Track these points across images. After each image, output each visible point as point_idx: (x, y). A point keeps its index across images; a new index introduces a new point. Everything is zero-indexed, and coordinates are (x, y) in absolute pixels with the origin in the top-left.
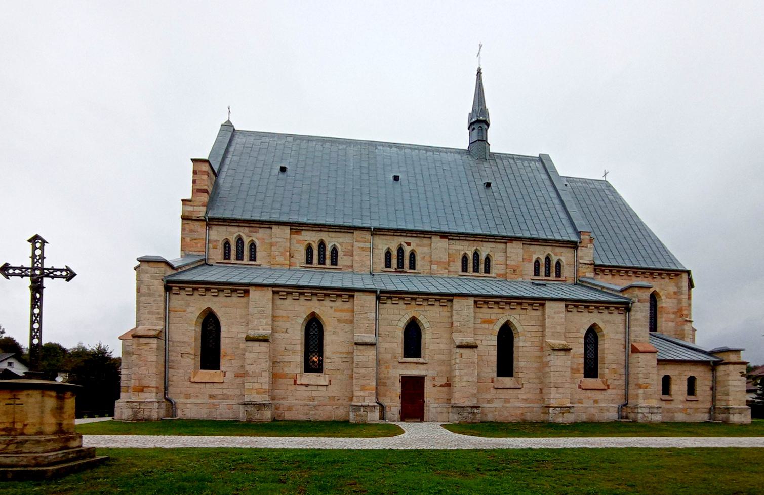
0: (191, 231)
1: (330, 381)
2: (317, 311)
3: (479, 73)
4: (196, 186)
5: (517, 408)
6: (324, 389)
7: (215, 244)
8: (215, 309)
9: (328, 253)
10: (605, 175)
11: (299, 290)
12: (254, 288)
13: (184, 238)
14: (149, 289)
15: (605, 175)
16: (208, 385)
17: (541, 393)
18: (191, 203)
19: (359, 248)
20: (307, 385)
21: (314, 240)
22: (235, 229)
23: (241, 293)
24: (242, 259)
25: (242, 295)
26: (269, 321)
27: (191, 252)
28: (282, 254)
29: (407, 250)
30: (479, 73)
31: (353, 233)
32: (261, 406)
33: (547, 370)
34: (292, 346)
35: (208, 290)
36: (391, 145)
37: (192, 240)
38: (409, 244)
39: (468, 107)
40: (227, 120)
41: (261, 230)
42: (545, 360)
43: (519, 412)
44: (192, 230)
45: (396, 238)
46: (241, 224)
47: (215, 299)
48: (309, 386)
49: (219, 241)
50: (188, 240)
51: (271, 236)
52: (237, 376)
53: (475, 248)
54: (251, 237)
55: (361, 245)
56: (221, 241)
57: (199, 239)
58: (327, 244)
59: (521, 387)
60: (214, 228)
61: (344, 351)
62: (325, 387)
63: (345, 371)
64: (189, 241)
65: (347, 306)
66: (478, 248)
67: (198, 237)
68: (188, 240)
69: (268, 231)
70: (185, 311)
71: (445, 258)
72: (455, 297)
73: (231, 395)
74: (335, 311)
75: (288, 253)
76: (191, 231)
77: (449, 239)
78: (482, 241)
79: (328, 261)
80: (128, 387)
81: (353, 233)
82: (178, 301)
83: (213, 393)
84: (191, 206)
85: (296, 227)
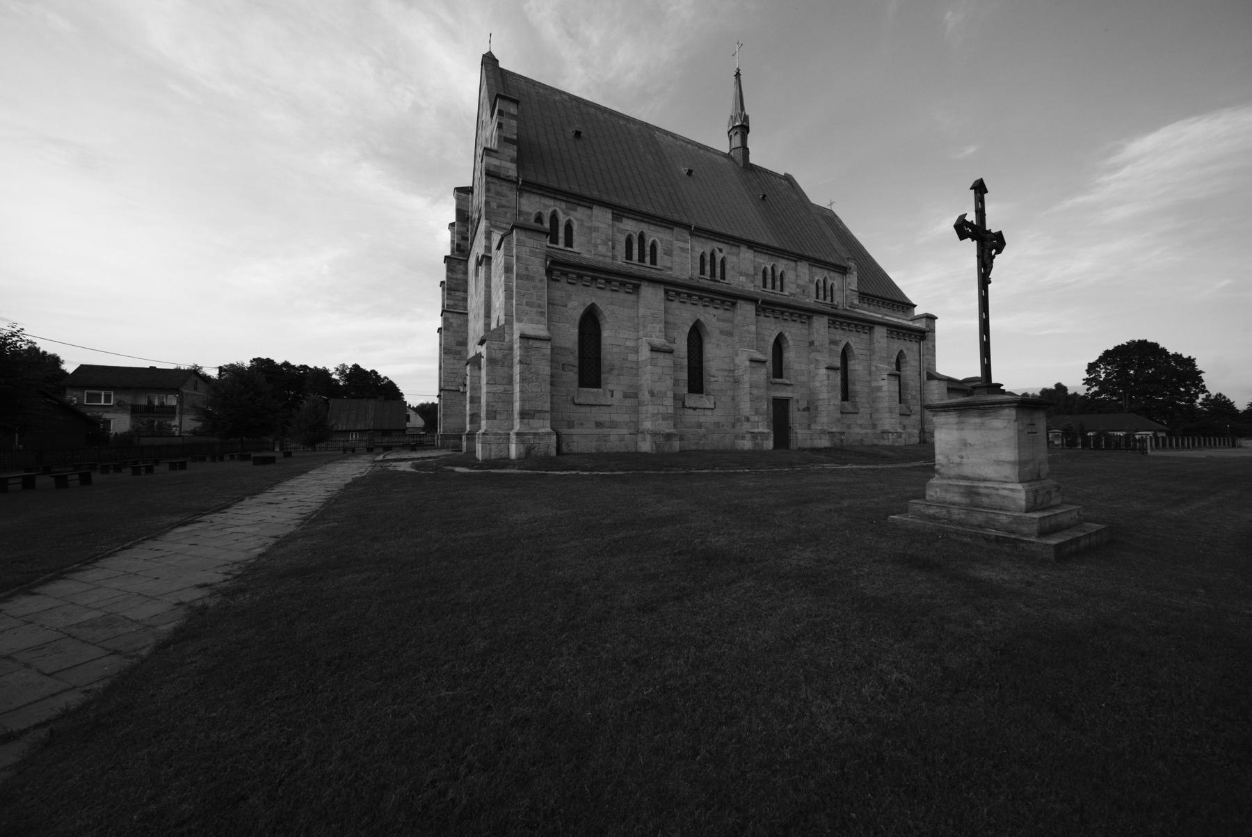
0: (498, 194)
1: (715, 403)
2: (702, 319)
3: (738, 75)
4: (503, 132)
5: (858, 434)
6: (708, 412)
7: (526, 217)
8: (601, 305)
9: (648, 249)
10: (831, 204)
11: (677, 289)
12: (646, 284)
13: (489, 202)
14: (527, 269)
15: (831, 204)
16: (594, 409)
17: (871, 418)
18: (498, 155)
19: (679, 247)
20: (695, 409)
21: (635, 231)
22: (550, 202)
23: (629, 288)
24: (557, 243)
25: (631, 291)
26: (662, 326)
27: (499, 223)
28: (605, 243)
29: (719, 256)
30: (738, 75)
31: (672, 229)
32: (669, 437)
33: (879, 394)
34: (681, 360)
35: (594, 279)
36: (667, 133)
37: (499, 206)
38: (721, 251)
39: (729, 108)
40: (488, 51)
41: (580, 209)
42: (874, 384)
43: (859, 438)
44: (498, 192)
45: (710, 241)
46: (558, 197)
47: (599, 292)
48: (698, 410)
49: (531, 214)
50: (494, 205)
51: (590, 217)
52: (626, 396)
53: (772, 263)
54: (568, 215)
55: (681, 244)
56: (533, 215)
57: (509, 207)
58: (647, 239)
59: (712, 406)
60: (526, 195)
61: (726, 367)
62: (711, 411)
63: (729, 391)
64: (495, 207)
65: (728, 315)
66: (776, 263)
67: (507, 204)
68: (494, 205)
69: (587, 212)
70: (566, 306)
71: (751, 271)
72: (814, 315)
73: (620, 422)
74: (718, 320)
75: (610, 243)
76: (498, 194)
77: (755, 251)
78: (778, 256)
79: (648, 259)
80: (496, 411)
81: (672, 229)
82: (563, 289)
83: (601, 419)
84: (498, 159)
85: (620, 212)
